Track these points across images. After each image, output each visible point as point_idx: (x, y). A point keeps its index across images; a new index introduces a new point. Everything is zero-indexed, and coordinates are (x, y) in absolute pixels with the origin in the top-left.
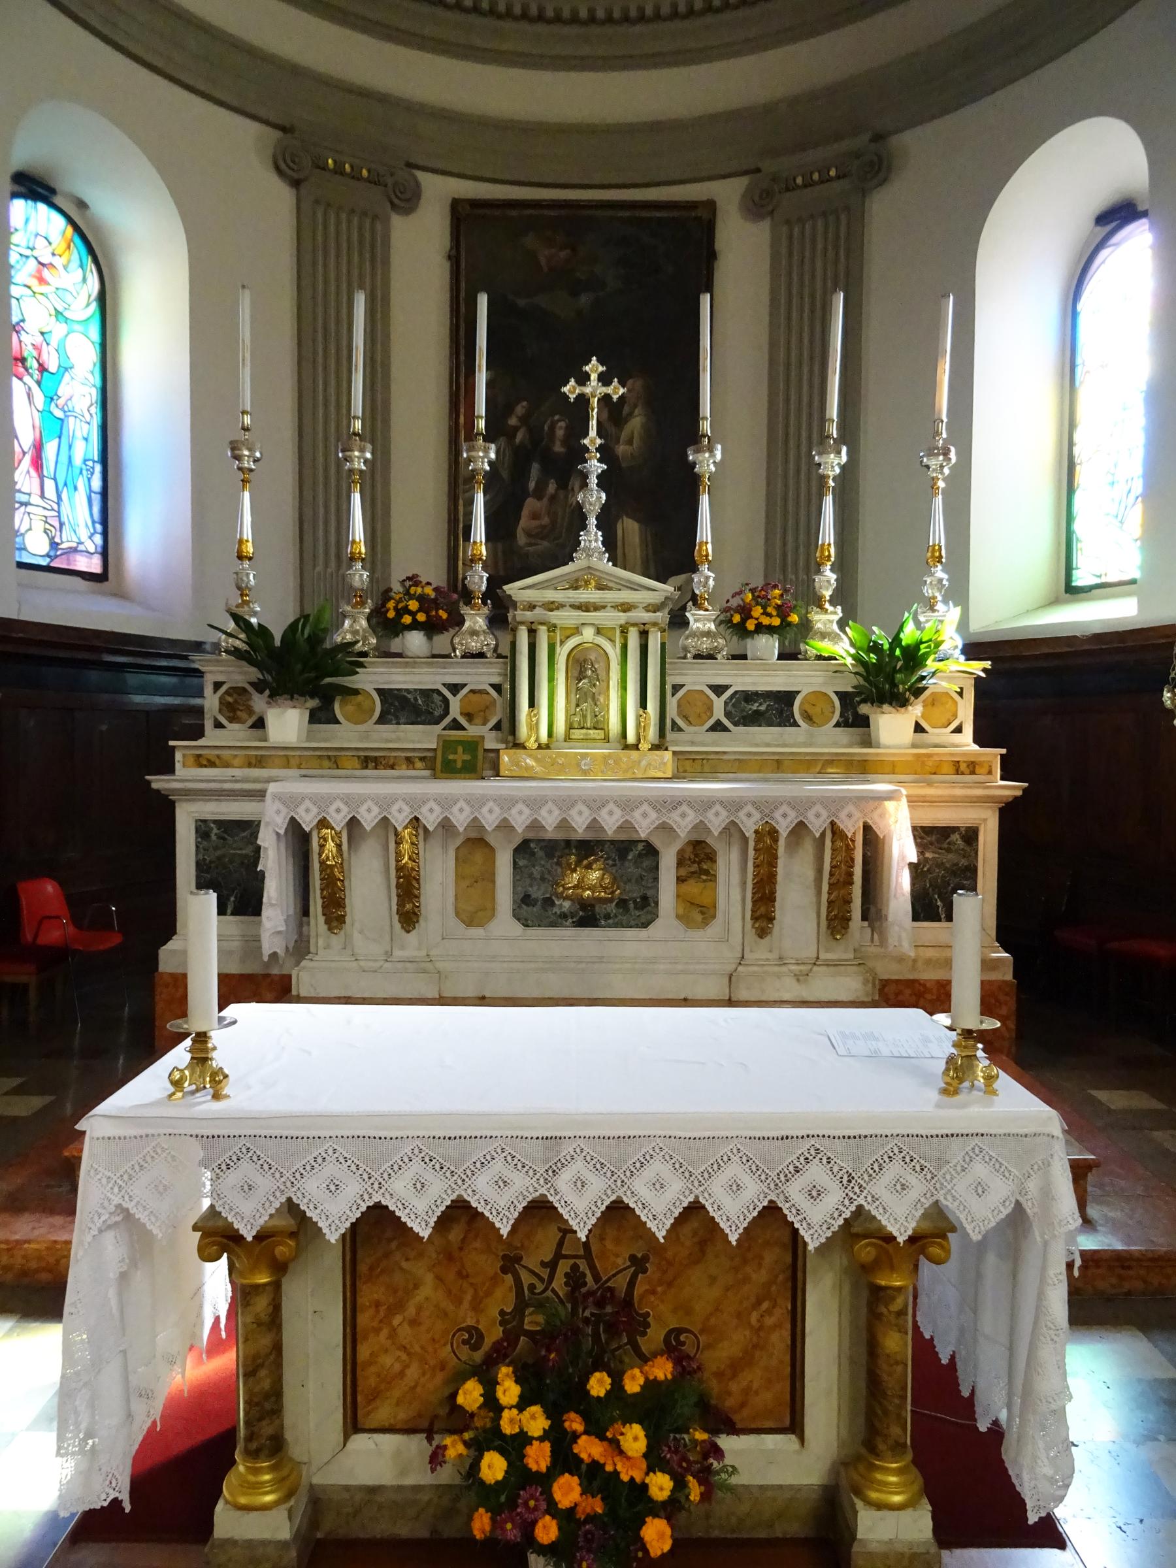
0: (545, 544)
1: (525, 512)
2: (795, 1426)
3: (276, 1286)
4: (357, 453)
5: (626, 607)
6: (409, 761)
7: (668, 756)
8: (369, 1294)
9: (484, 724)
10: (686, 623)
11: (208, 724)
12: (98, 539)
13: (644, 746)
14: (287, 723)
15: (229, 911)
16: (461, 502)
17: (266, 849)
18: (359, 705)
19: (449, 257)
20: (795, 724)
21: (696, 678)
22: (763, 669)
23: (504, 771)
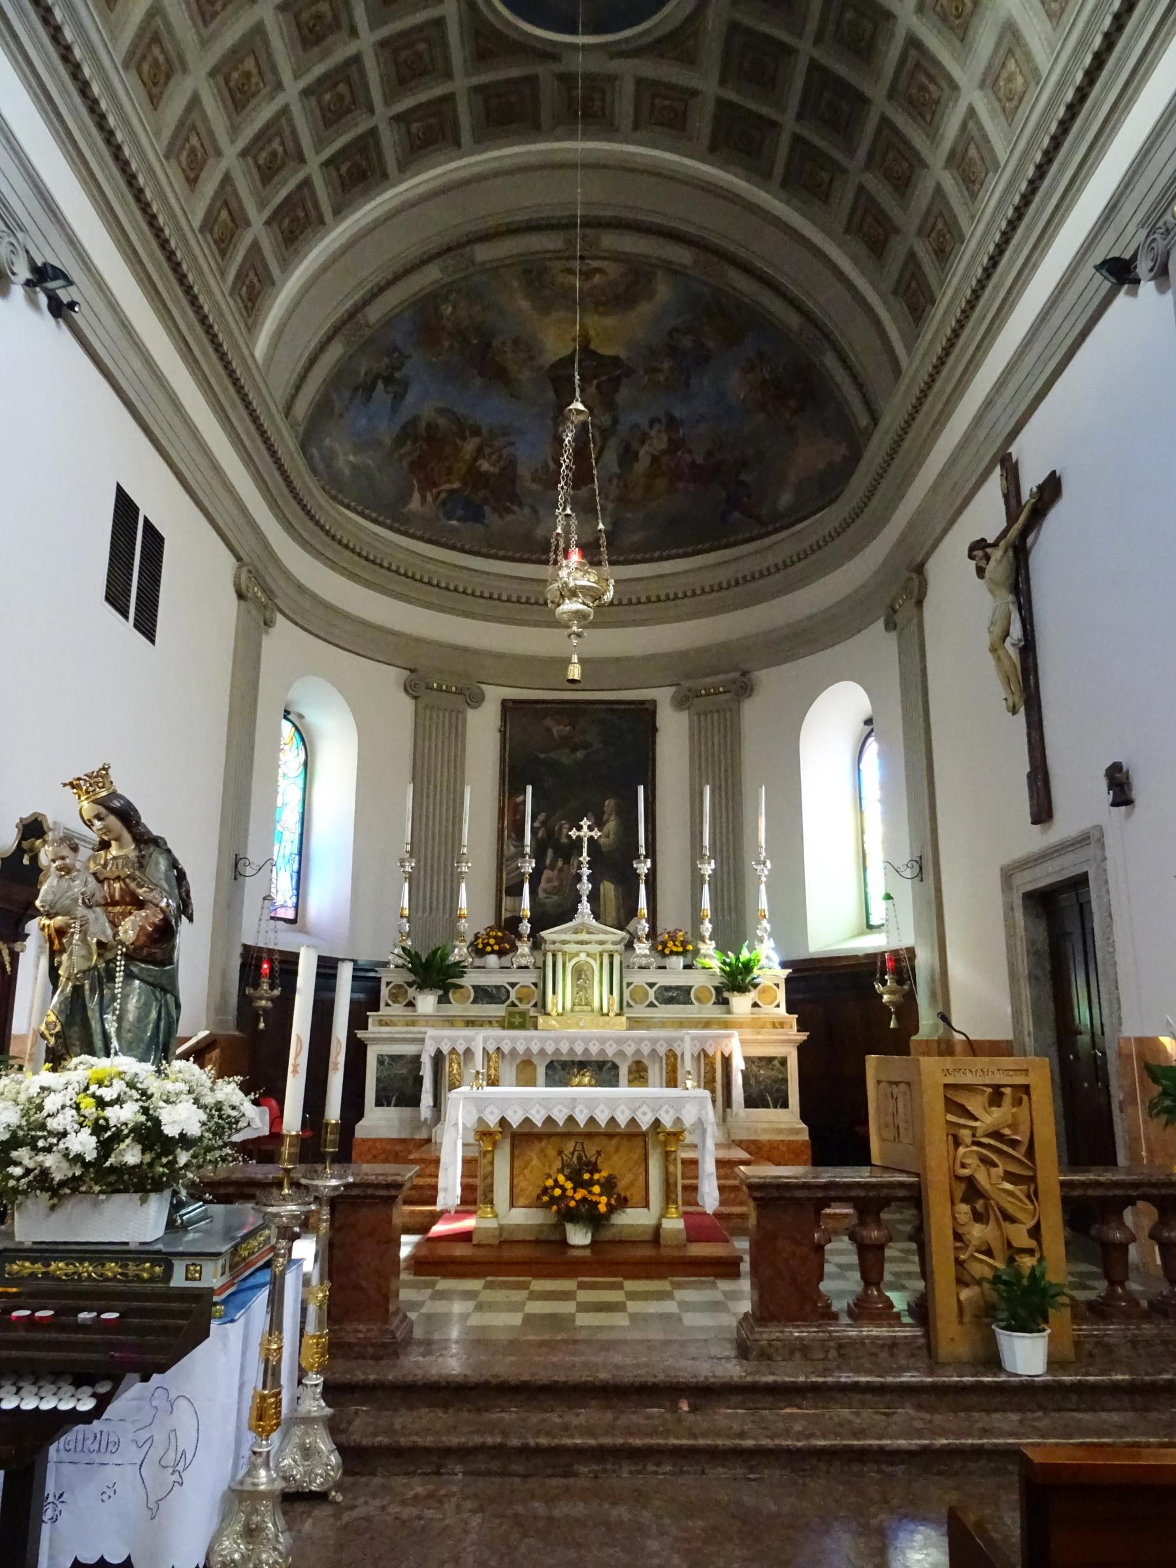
0: (555, 898)
2: (647, 1206)
3: (493, 1151)
5: (602, 943)
7: (624, 1019)
8: (517, 1152)
10: (634, 949)
11: (382, 1004)
12: (294, 899)
13: (612, 1014)
14: (427, 1002)
15: (393, 1102)
20: (692, 1003)
21: (639, 979)
22: (675, 974)
23: (539, 1027)
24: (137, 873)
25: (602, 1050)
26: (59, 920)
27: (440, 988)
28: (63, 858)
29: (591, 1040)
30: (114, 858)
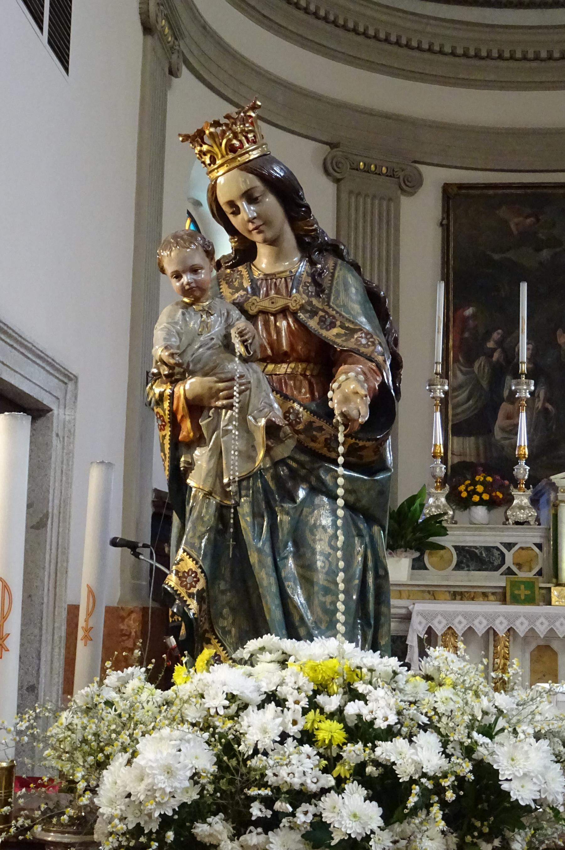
1: (501, 414)
4: (439, 387)
6: (485, 595)
9: (530, 571)
16: (450, 406)
17: (411, 646)
18: (442, 557)
19: (441, 225)
24: (315, 302)
25: (552, 629)
26: (190, 386)
27: (417, 550)
28: (194, 270)
29: (517, 618)
30: (267, 277)
